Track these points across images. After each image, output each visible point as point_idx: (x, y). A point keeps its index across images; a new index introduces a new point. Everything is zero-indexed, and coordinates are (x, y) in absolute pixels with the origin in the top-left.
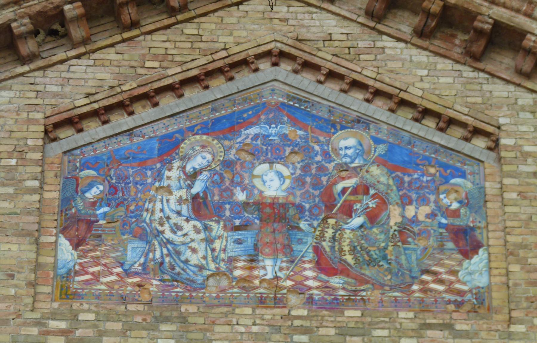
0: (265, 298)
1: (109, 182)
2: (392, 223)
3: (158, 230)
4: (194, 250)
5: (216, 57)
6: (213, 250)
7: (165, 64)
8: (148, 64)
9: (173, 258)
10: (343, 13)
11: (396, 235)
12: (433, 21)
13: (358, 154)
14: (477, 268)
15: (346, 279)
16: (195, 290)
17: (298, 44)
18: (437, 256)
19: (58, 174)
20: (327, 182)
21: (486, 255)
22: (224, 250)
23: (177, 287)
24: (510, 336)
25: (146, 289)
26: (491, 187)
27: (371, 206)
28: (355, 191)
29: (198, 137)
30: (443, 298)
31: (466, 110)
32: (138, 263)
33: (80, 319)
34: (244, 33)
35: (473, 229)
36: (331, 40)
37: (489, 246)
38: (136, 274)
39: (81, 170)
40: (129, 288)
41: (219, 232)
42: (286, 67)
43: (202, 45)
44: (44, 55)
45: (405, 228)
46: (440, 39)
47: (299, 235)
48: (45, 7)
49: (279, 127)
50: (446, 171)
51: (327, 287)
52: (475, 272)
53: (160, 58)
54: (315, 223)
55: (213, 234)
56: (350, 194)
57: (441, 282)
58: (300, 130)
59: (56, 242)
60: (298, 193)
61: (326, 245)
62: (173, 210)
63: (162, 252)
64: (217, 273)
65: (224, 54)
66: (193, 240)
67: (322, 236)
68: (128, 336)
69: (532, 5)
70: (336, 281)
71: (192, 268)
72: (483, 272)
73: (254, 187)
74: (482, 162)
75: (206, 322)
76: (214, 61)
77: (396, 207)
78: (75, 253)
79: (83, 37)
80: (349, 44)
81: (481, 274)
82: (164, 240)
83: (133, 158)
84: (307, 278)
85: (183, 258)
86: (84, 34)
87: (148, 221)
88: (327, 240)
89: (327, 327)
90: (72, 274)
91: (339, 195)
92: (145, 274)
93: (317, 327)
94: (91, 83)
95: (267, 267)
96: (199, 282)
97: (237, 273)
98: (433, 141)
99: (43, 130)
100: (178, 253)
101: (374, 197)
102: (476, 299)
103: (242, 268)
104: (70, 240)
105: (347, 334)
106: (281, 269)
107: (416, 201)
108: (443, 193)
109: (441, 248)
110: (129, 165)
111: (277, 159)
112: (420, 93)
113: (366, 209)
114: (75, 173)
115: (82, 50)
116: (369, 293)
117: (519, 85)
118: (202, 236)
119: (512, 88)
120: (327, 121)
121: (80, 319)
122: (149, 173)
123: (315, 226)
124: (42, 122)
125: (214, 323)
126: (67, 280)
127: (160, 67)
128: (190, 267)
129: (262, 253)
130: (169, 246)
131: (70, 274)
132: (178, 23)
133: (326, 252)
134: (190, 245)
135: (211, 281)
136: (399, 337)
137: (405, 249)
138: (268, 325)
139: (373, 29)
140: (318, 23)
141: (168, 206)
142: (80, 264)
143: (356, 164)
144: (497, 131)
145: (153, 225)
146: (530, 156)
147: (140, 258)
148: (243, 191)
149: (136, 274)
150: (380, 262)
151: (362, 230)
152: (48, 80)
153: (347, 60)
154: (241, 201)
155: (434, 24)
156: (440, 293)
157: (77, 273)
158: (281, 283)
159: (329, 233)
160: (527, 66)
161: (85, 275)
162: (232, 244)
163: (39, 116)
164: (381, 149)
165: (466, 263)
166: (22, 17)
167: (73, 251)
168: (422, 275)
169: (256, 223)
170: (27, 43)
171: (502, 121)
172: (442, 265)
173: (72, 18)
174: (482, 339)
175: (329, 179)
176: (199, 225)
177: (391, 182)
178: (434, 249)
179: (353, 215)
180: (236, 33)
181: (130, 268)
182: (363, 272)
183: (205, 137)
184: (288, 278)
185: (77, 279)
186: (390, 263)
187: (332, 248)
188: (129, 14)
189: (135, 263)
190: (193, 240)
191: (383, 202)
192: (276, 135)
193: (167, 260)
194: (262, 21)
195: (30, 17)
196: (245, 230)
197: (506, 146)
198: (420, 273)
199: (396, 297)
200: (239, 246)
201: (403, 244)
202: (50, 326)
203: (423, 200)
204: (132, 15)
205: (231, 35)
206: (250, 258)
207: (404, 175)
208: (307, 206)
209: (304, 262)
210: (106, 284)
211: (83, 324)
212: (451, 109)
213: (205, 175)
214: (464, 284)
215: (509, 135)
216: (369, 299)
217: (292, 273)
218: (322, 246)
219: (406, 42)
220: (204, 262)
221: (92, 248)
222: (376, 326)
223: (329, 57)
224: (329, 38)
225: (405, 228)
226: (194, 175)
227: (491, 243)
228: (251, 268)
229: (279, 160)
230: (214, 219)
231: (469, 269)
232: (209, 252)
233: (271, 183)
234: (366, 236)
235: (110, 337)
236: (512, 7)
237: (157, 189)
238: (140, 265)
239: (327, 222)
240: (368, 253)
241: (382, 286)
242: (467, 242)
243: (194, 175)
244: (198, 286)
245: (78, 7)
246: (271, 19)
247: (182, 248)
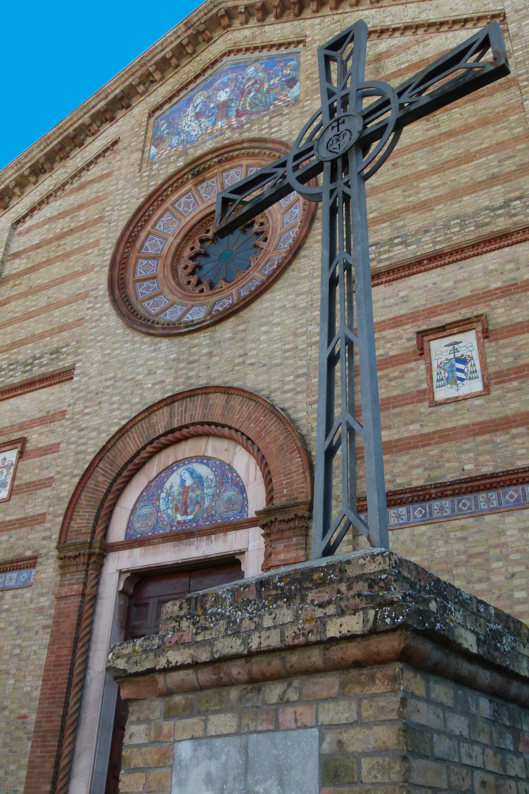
42: (232, 55)
64: (202, 134)
203: (277, 76)
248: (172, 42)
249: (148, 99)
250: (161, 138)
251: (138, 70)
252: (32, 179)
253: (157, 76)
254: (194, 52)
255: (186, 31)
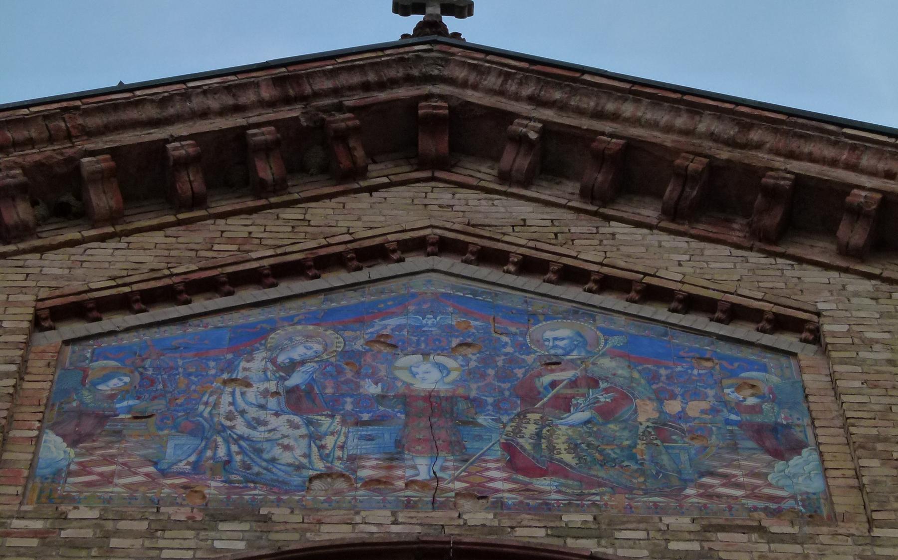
0: (415, 502)
1: (141, 374)
2: (642, 418)
3: (223, 425)
4: (287, 448)
5: (331, 241)
6: (321, 447)
7: (246, 247)
8: (216, 247)
9: (247, 455)
10: (543, 197)
11: (650, 433)
12: (692, 188)
13: (576, 346)
14: (802, 471)
15: (562, 481)
16: (286, 492)
17: (471, 229)
18: (726, 456)
19: (53, 363)
20: (524, 375)
21: (815, 456)
22: (342, 448)
23: (255, 488)
24: (874, 541)
25: (196, 492)
26: (814, 380)
27: (602, 400)
28: (573, 383)
29: (299, 327)
30: (743, 504)
31: (760, 295)
32: (185, 462)
33: (69, 517)
34: (382, 218)
35: (788, 426)
36: (524, 225)
37: (819, 444)
38: (181, 474)
39: (92, 361)
40: (166, 490)
41: (332, 427)
43: (309, 229)
44: (44, 235)
45: (665, 425)
46: (705, 223)
47: (476, 431)
48: (51, 157)
49: (438, 318)
50: (732, 365)
51: (528, 490)
52: (800, 475)
53: (239, 241)
54: (505, 419)
55: (323, 429)
56: (565, 387)
57: (738, 486)
58: (476, 320)
59: (38, 438)
60: (474, 386)
61: (526, 443)
62: (252, 404)
63: (229, 450)
65: (348, 238)
66: (284, 436)
67: (518, 431)
68: (158, 538)
69: (857, 152)
70: (543, 484)
71: (283, 468)
72: (812, 475)
73: (396, 378)
74: (794, 355)
75: (306, 521)
76: (329, 245)
77: (648, 402)
78: (72, 452)
79: (111, 208)
80: (555, 230)
81: (809, 477)
82: (235, 436)
83: (185, 348)
84: (492, 480)
85: (266, 456)
86: (112, 203)
87: (206, 414)
88: (527, 436)
89: (530, 527)
90: (63, 475)
91: (545, 388)
92: (197, 474)
93: (512, 528)
94: (119, 266)
95: (419, 467)
96: (295, 483)
97: (364, 473)
98: (706, 332)
99: (30, 317)
100: (259, 452)
101: (606, 391)
102: (803, 506)
103: (373, 468)
104: (64, 437)
105: (567, 536)
106: (443, 469)
107: (682, 395)
108: (729, 387)
109: (734, 448)
110: (178, 355)
111: (435, 350)
112: (679, 277)
113: (595, 403)
114: (83, 364)
115: (109, 229)
116: (606, 498)
117: (846, 270)
118: (303, 431)
119: (834, 274)
120: (521, 312)
121: (69, 517)
122: (212, 364)
123: (505, 421)
124: (34, 304)
125: (320, 522)
126: (53, 482)
127: (239, 250)
128: (279, 466)
129: (409, 450)
130: (242, 443)
131: (58, 475)
132: (271, 206)
133: (525, 450)
134: (280, 442)
135: (317, 484)
136: (666, 540)
137: (667, 448)
138: (421, 524)
139: (595, 214)
140: (502, 210)
141: (244, 400)
142: (80, 463)
143: (575, 355)
144: (815, 318)
145: (216, 419)
146: (877, 343)
147: (189, 456)
148: (376, 384)
149: (181, 474)
150: (623, 462)
151: (589, 425)
152: (47, 262)
153: (553, 245)
154: (373, 395)
155: (695, 193)
156: (737, 498)
157: (70, 474)
158: (442, 485)
159: (531, 429)
160: (857, 237)
161: (85, 475)
162: (356, 441)
163: (30, 298)
164: (616, 341)
165: (780, 465)
166: (11, 168)
167: (68, 449)
168: (700, 477)
169: (400, 418)
170: (15, 207)
171: (821, 306)
172: (739, 467)
173: (93, 173)
174: (822, 544)
175: (527, 371)
176: (297, 419)
177: (636, 375)
178: (720, 448)
179: (572, 409)
180: (364, 218)
181: (169, 468)
182: (592, 472)
183: (311, 327)
184: (457, 479)
185: (71, 480)
186: (642, 464)
187: (537, 446)
188: (190, 182)
189: (181, 461)
190: (284, 436)
191: (624, 397)
192: (433, 325)
193: (238, 458)
194: (411, 207)
195: (22, 167)
196: (379, 425)
197: (834, 335)
198: (696, 475)
199: (655, 503)
200: (369, 442)
201: (663, 442)
202: (12, 526)
204: (195, 185)
205: (359, 219)
206: (388, 456)
207: (659, 367)
208: (490, 400)
209: (486, 461)
210: (125, 486)
211: (75, 524)
212: (732, 294)
213: (309, 367)
214: (782, 488)
215: (835, 320)
216: (606, 505)
217: (464, 474)
218: (518, 444)
219: (650, 227)
220: (305, 461)
221: (103, 444)
222: (622, 527)
223: (523, 242)
224: (522, 223)
225: (665, 425)
226: (293, 366)
227: (821, 440)
228: (390, 468)
229: (439, 352)
230: (325, 413)
231: (786, 471)
232: (315, 449)
233: (426, 376)
234: (595, 432)
235: (124, 538)
236: (824, 158)
237: (225, 382)
238: (188, 463)
239: (525, 416)
240: (601, 452)
241: (630, 490)
242: (780, 443)
243: (293, 366)
244: (293, 488)
245: (105, 160)
246: (426, 205)
247: (266, 446)
248: (204, 114)
249: (33, 259)
250: (102, 419)
251: (30, 142)
252: (516, 160)
253: (191, 181)
254: (279, 187)
255: (271, 104)
